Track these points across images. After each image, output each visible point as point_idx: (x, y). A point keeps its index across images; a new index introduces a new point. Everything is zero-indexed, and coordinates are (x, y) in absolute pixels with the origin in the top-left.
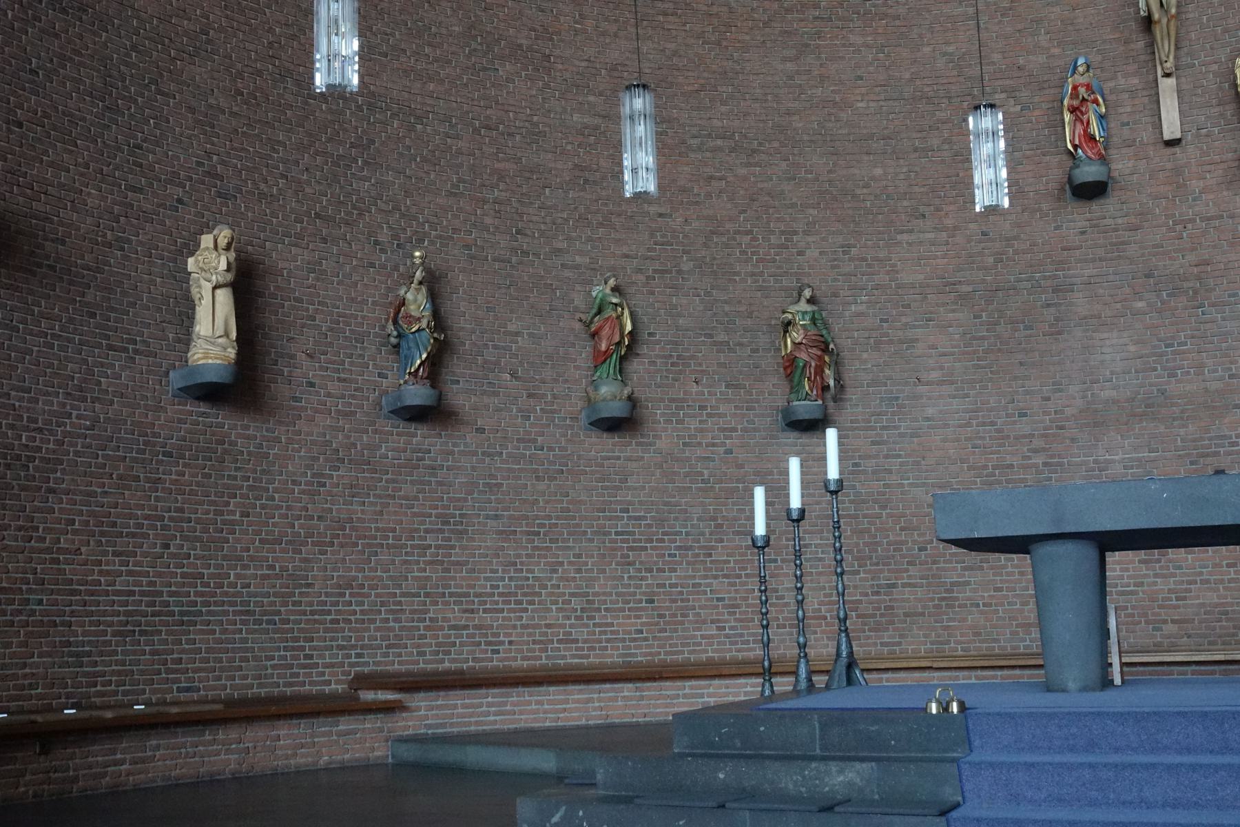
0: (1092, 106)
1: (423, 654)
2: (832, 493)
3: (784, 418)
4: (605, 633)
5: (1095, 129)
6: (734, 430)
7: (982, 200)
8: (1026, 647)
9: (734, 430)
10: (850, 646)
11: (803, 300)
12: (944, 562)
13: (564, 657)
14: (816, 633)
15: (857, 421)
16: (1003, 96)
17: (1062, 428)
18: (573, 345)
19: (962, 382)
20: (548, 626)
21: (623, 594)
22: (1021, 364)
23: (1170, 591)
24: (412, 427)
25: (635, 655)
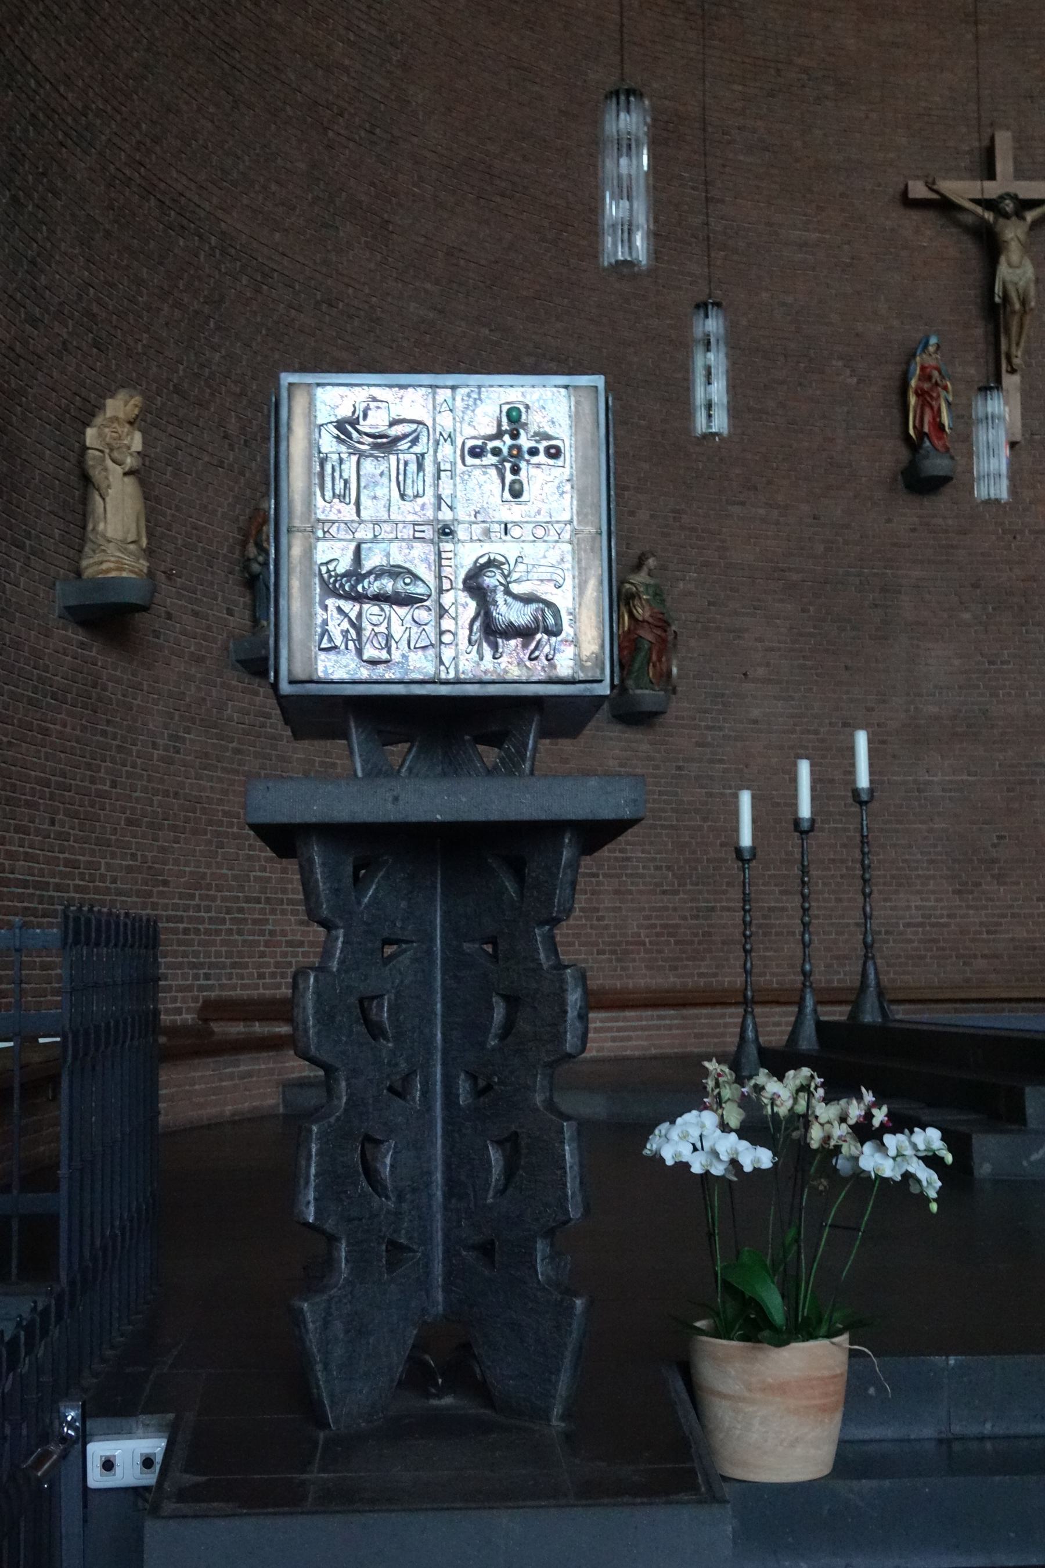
0: (943, 393)
1: (261, 976)
2: (862, 803)
8: (839, 981)
11: (645, 569)
12: (763, 885)
14: (634, 960)
16: (840, 363)
17: (884, 742)
19: (787, 682)
22: (847, 668)
23: (981, 924)
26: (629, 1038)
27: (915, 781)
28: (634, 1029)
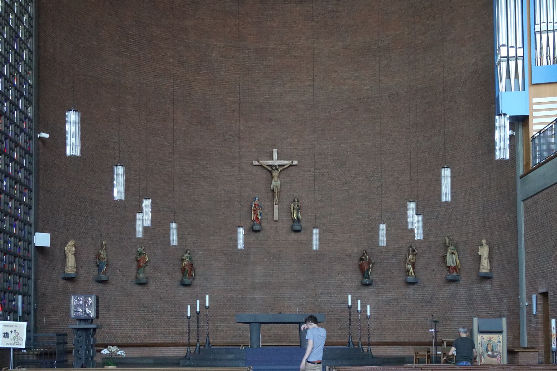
0: (258, 211)
3: (181, 283)
4: (138, 335)
5: (259, 216)
6: (168, 285)
7: (239, 247)
9: (168, 285)
10: (209, 340)
11: (187, 253)
13: (129, 341)
15: (198, 284)
18: (132, 263)
20: (126, 333)
21: (142, 326)
23: (267, 329)
24: (99, 284)
25: (144, 341)
26: (180, 352)
27: (253, 297)
28: (181, 351)
